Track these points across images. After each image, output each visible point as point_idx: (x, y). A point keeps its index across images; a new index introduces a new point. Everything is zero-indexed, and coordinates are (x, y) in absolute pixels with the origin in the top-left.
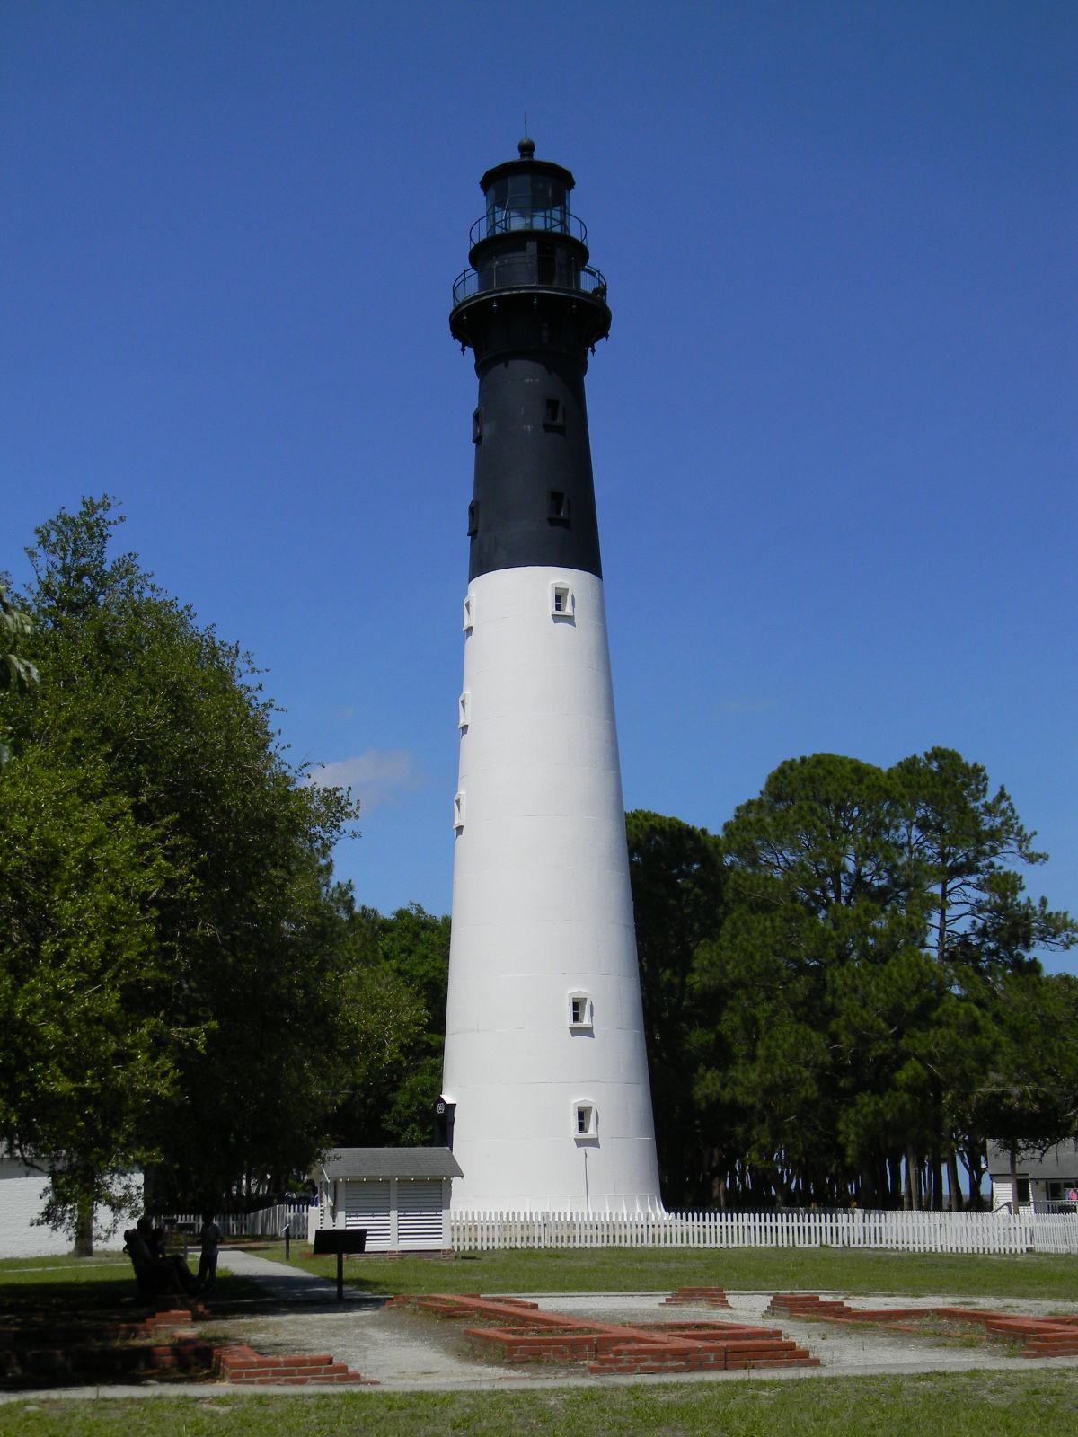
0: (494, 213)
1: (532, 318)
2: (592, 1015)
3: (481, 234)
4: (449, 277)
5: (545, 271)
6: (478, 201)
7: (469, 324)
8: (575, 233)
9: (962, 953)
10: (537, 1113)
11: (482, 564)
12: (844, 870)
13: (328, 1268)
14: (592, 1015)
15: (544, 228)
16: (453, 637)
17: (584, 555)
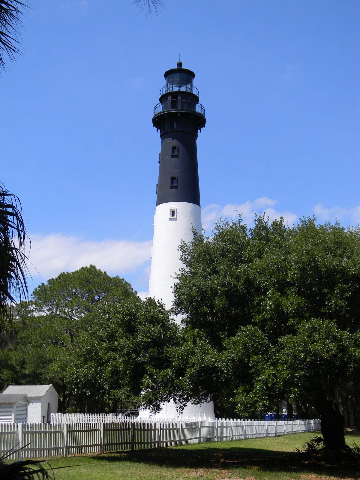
0: (168, 85)
1: (180, 120)
3: (164, 92)
4: (152, 105)
7: (159, 121)
8: (195, 92)
9: (278, 265)
13: (275, 343)
15: (185, 91)
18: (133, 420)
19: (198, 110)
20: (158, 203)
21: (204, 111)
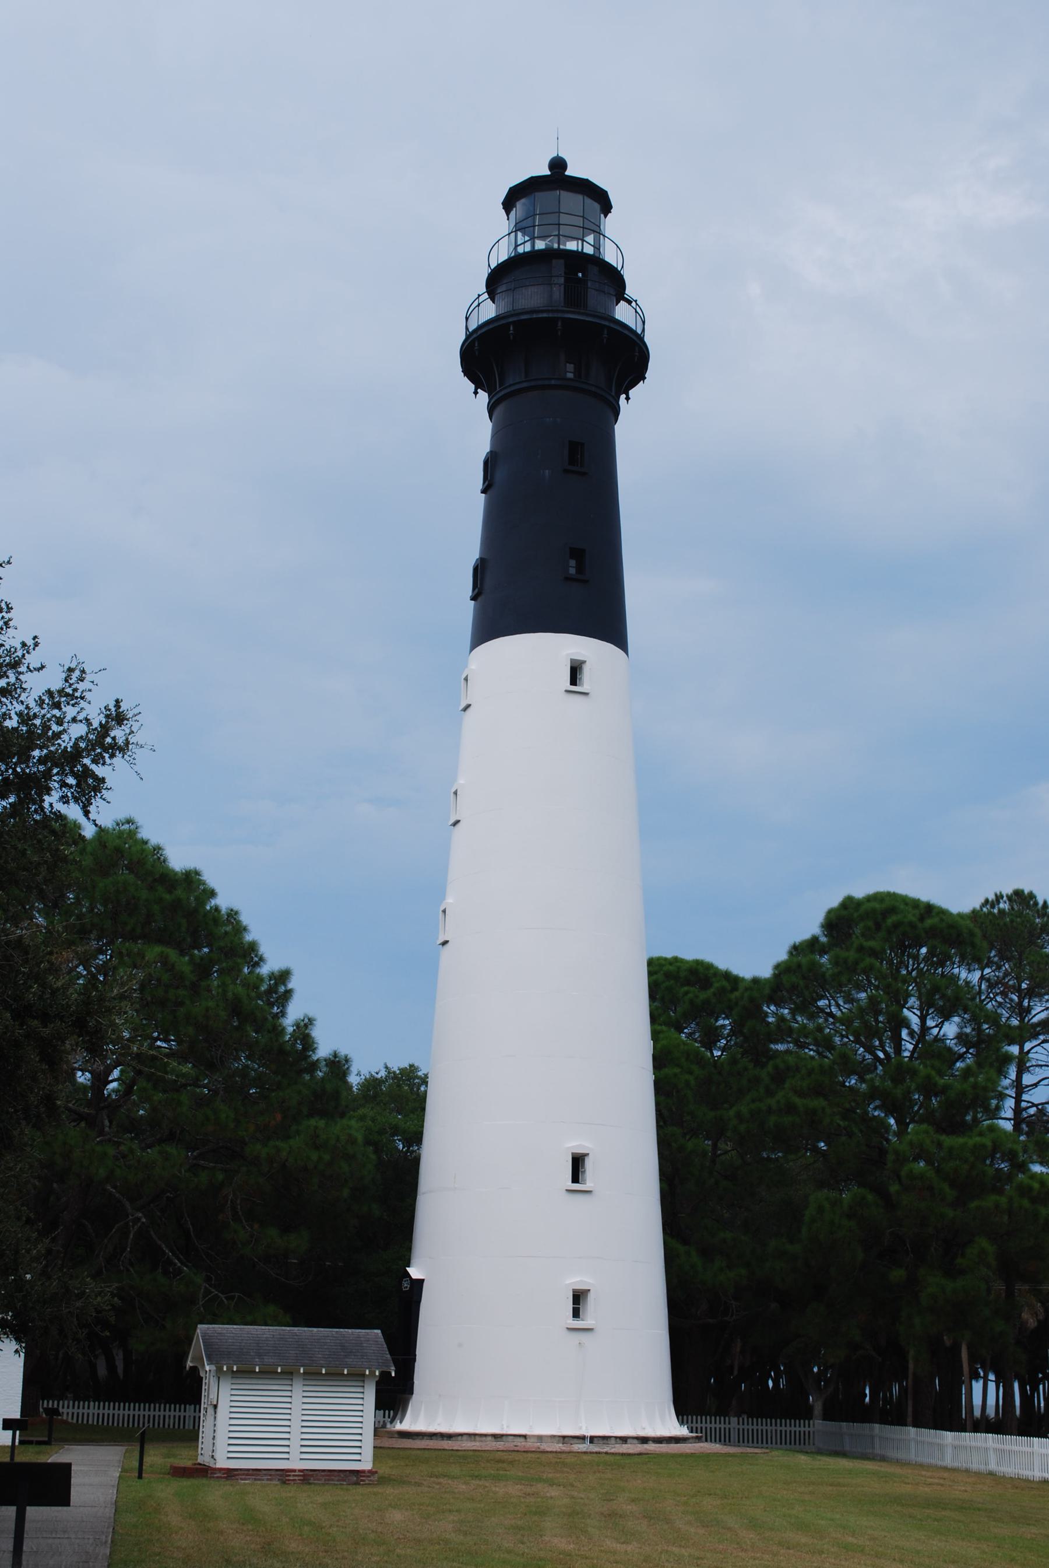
3: (503, 254)
4: (458, 300)
5: (575, 294)
6: (501, 223)
8: (610, 256)
11: (487, 629)
12: (906, 1023)
18: (937, 1078)
19: (622, 313)
21: (644, 323)
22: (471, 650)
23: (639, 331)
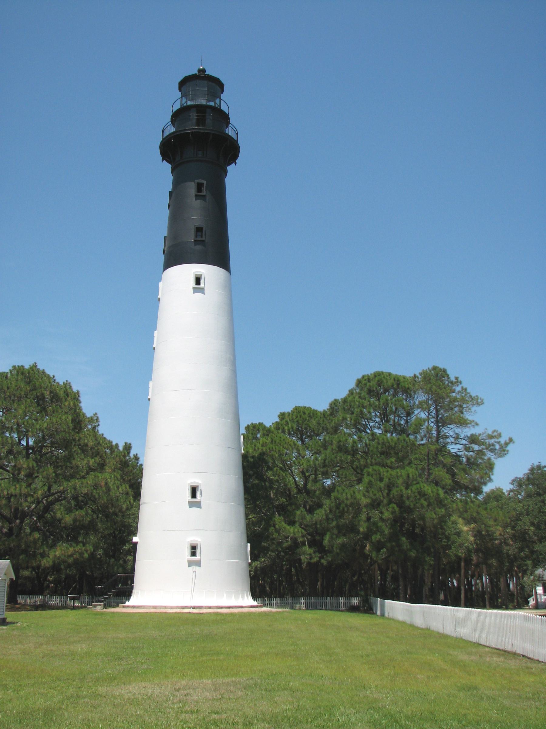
1: (200, 145)
2: (201, 494)
3: (177, 106)
4: (159, 124)
7: (170, 149)
8: (224, 108)
10: (187, 557)
14: (201, 494)
16: (152, 304)
17: (221, 259)
19: (229, 131)
20: (168, 264)
22: (163, 271)
23: (236, 139)
